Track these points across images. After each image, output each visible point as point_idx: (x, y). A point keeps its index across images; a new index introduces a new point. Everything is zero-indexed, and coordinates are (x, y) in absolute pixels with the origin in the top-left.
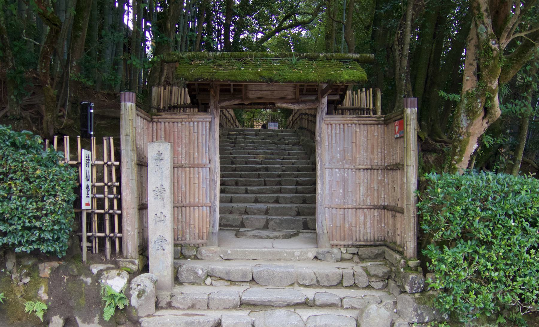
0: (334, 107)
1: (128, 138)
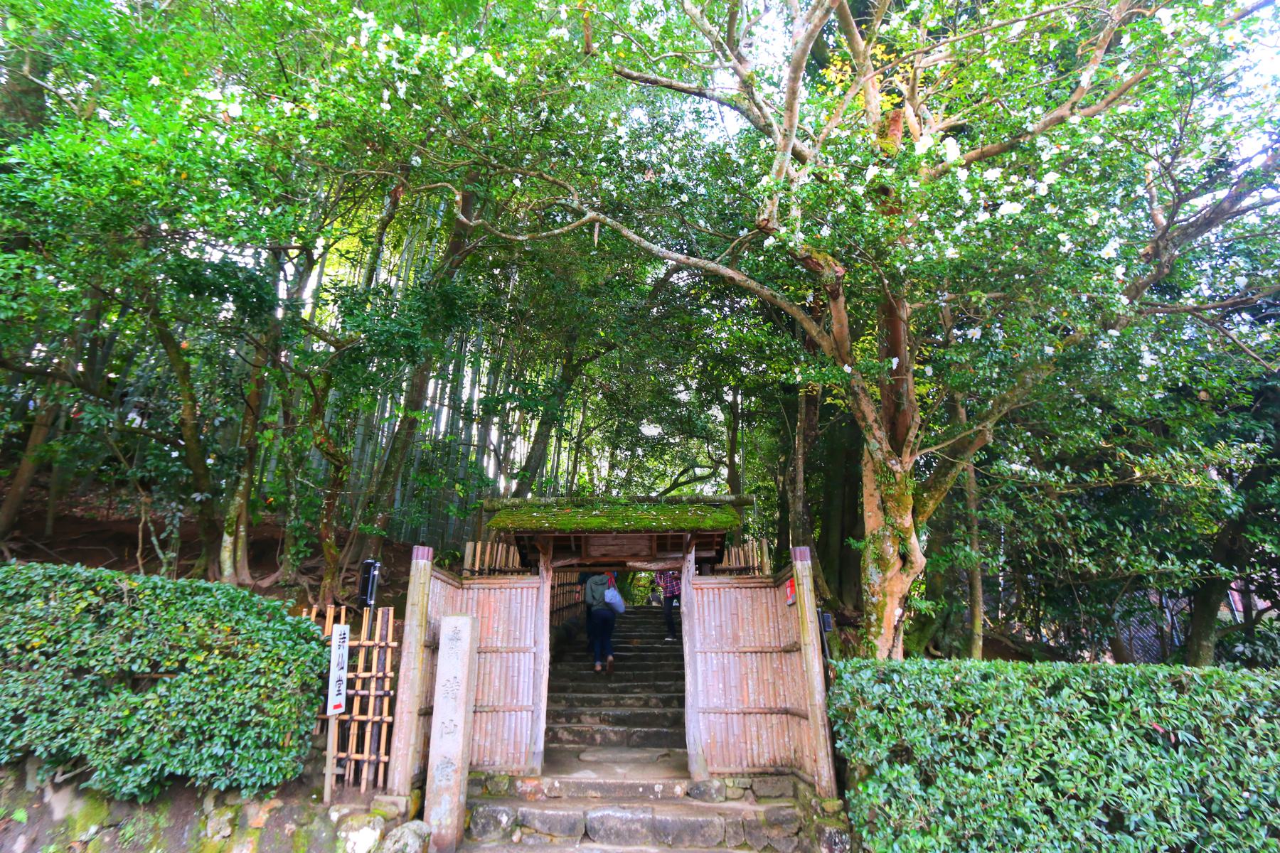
0: (706, 567)
1: (416, 608)
